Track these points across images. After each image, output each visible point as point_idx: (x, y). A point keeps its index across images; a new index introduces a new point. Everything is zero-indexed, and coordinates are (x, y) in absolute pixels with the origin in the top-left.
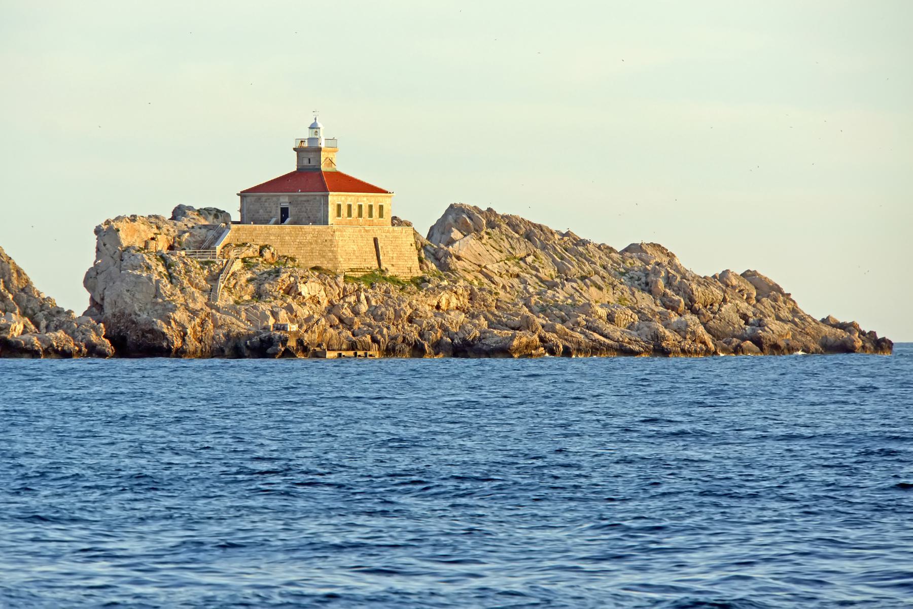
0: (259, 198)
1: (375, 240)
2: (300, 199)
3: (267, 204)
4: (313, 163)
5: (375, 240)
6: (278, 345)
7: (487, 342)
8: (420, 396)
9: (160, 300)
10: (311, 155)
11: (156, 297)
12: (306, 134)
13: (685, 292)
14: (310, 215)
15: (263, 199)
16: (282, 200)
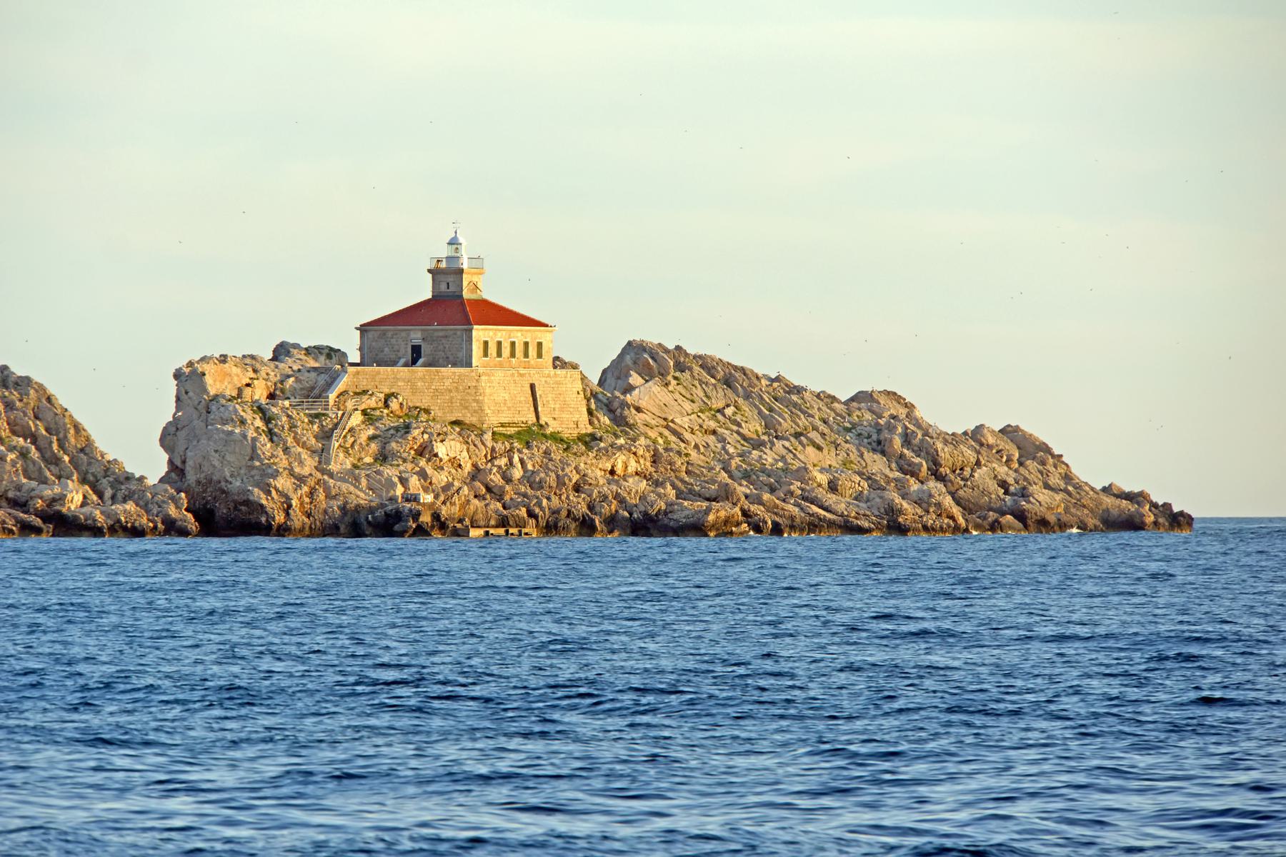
0: (384, 333)
1: (532, 387)
2: (436, 334)
3: (393, 341)
4: (452, 289)
5: (532, 387)
6: (407, 521)
9: (257, 464)
10: (451, 279)
12: (444, 252)
13: (927, 453)
14: (449, 354)
15: (389, 334)
16: (413, 335)
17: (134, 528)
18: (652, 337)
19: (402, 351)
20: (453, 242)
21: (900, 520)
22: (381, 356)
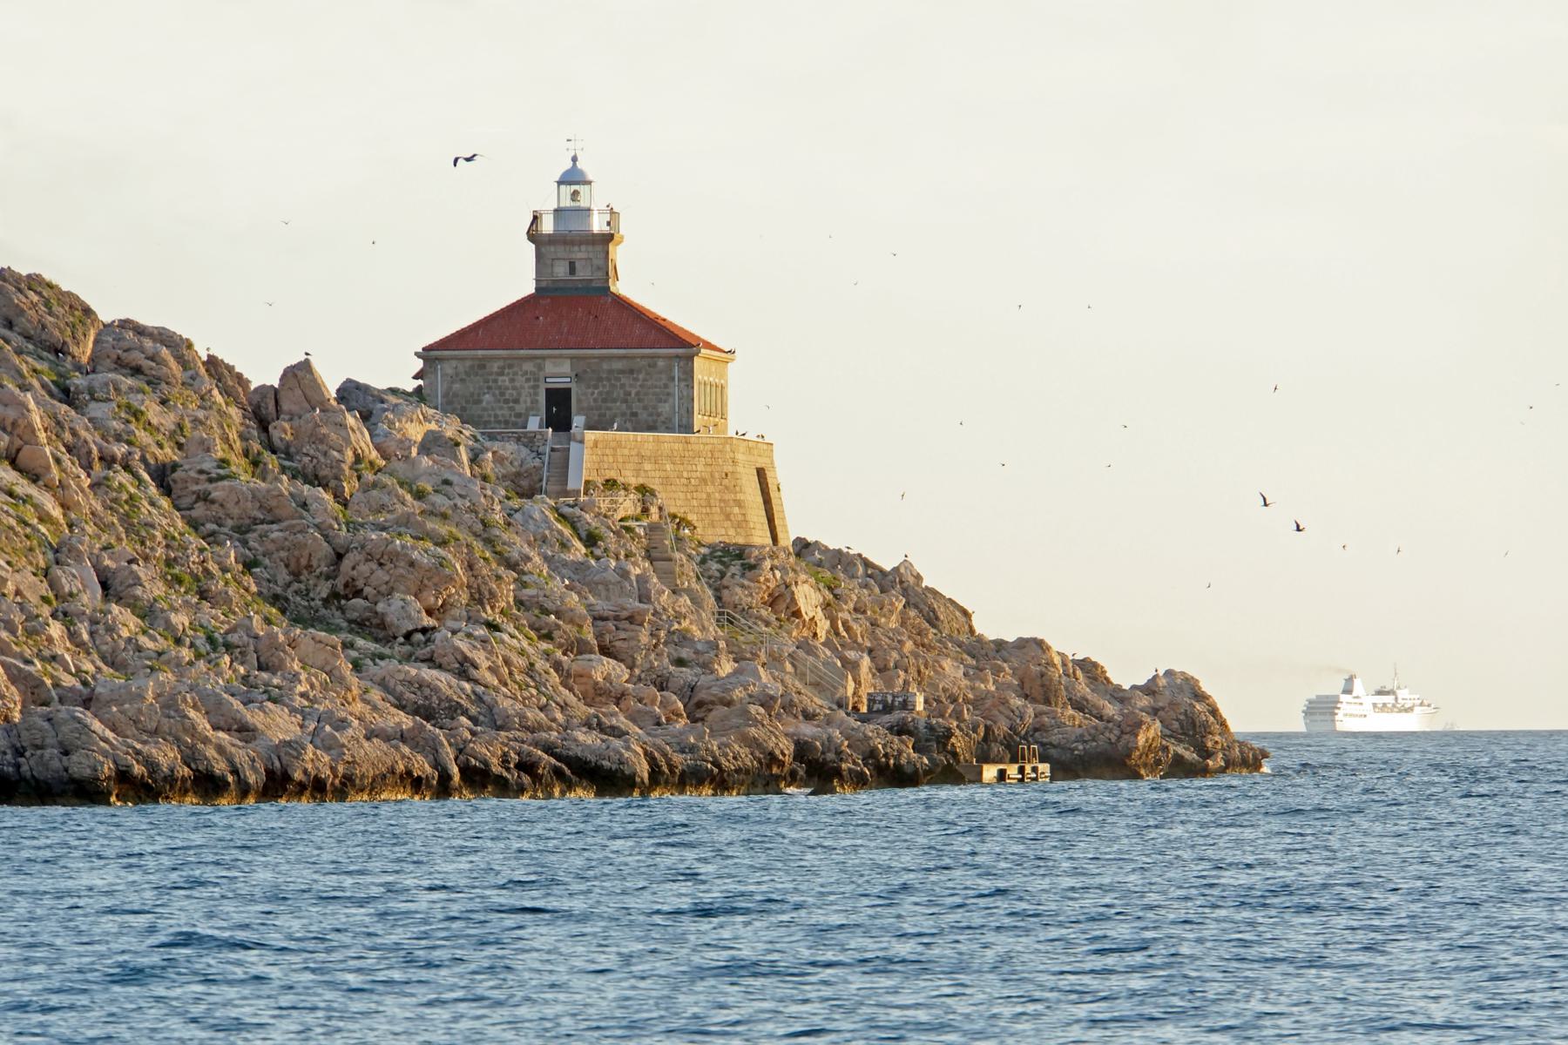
0: (482, 364)
2: (605, 366)
3: (504, 380)
4: (583, 273)
7: (1055, 739)
8: (896, 1013)
10: (580, 254)
12: (548, 199)
14: (637, 407)
16: (549, 367)
17: (898, 767)
18: (361, 379)
20: (573, 178)
21: (1210, 744)
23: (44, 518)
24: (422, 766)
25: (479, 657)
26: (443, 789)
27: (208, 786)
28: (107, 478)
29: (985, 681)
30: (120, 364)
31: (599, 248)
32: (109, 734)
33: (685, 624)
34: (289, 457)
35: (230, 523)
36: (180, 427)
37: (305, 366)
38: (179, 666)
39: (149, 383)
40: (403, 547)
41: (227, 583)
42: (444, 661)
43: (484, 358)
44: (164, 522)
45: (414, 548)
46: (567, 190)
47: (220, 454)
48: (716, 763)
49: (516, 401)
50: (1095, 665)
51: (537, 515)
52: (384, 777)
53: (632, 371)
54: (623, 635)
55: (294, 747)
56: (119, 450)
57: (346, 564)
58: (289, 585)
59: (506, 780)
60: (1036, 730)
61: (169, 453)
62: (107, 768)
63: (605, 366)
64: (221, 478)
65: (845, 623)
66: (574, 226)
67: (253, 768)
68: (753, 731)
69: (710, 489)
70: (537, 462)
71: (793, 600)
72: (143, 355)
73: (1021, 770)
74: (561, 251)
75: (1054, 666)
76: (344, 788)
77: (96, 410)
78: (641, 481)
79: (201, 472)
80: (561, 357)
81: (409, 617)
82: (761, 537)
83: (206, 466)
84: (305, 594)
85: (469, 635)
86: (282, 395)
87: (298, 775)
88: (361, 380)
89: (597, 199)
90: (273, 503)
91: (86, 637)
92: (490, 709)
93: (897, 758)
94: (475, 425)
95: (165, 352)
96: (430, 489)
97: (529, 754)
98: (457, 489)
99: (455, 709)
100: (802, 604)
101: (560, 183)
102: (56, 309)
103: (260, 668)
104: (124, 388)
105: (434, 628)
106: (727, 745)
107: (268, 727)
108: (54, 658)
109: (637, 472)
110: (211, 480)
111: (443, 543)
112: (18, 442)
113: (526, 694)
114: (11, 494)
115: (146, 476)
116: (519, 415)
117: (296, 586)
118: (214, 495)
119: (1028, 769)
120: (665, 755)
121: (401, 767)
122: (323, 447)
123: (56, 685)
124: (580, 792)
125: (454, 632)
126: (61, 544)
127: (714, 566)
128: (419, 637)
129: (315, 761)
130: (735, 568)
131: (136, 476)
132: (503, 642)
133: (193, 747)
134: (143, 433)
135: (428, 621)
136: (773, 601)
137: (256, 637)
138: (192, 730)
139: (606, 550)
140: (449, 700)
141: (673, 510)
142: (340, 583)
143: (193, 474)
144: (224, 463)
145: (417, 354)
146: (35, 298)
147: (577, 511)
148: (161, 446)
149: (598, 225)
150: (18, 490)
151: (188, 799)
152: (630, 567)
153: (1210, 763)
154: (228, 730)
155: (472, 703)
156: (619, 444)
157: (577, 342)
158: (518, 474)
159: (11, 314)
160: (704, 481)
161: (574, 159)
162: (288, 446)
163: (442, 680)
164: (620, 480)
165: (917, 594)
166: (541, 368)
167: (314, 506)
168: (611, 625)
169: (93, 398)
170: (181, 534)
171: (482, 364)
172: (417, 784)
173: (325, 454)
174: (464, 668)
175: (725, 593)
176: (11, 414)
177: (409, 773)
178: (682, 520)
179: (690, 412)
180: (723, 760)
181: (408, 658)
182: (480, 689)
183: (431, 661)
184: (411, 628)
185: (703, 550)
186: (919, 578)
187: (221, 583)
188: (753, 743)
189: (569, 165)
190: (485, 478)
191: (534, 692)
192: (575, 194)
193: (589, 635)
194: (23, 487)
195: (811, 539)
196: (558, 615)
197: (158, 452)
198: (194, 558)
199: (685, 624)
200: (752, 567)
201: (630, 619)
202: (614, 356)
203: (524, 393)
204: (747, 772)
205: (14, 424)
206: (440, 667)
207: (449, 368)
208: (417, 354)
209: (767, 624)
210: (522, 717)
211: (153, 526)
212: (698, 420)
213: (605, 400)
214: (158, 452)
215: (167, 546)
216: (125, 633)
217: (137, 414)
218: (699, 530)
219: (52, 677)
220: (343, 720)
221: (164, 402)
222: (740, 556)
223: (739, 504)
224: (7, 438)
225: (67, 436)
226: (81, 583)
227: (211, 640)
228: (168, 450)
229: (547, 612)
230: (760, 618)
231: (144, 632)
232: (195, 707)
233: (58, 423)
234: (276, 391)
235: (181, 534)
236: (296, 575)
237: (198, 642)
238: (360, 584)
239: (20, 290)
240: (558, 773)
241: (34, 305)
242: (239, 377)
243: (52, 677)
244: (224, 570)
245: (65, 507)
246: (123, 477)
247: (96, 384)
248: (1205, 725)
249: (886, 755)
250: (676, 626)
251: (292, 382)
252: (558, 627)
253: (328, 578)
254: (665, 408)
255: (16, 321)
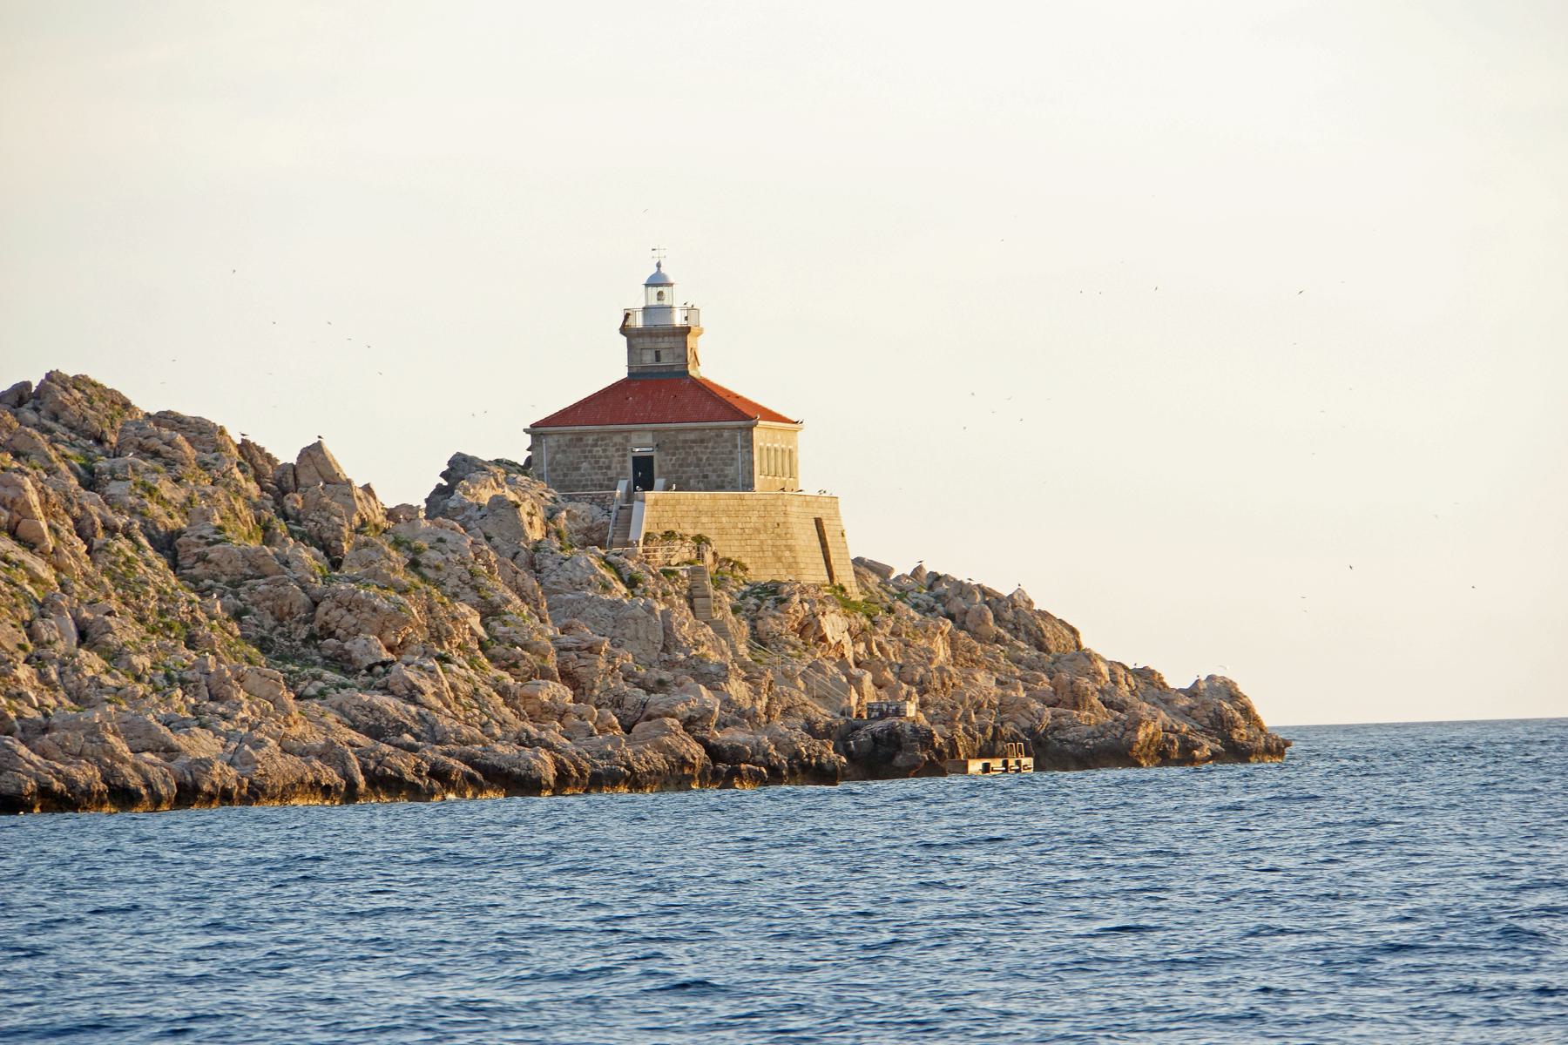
1: (818, 522)
2: (681, 437)
3: (598, 451)
4: (666, 361)
5: (818, 522)
6: (913, 749)
7: (1069, 736)
9: (682, 656)
10: (663, 344)
11: (665, 649)
12: (638, 299)
13: (1028, 633)
14: (708, 470)
15: (590, 440)
16: (634, 438)
17: (820, 765)
18: (469, 452)
19: (616, 467)
20: (657, 281)
21: (1235, 736)
22: (575, 476)
23: (35, 579)
24: (330, 776)
25: (426, 685)
26: (351, 795)
27: (123, 797)
28: (106, 545)
29: (1015, 689)
30: (142, 450)
31: (679, 339)
32: (35, 758)
33: (703, 650)
34: (299, 522)
35: (224, 578)
36: (190, 500)
37: (318, 447)
38: (134, 699)
39: (166, 464)
40: (367, 595)
41: (212, 629)
42: (396, 688)
43: (581, 433)
44: (158, 579)
45: (376, 596)
46: (655, 290)
47: (219, 522)
48: (629, 767)
49: (609, 468)
50: (1153, 672)
51: (583, 563)
52: (293, 786)
53: (702, 441)
54: (583, 662)
55: (206, 764)
56: (121, 521)
57: (321, 610)
58: (274, 629)
59: (418, 786)
60: (1056, 729)
61: (178, 522)
62: (30, 785)
63: (681, 437)
64: (217, 542)
65: (879, 645)
66: (660, 321)
67: (165, 782)
68: (667, 740)
69: (763, 537)
70: (605, 519)
71: (820, 628)
72: (184, 441)
73: (1005, 764)
74: (647, 342)
75: (1101, 674)
76: (255, 793)
77: (114, 488)
78: (698, 532)
79: (201, 537)
80: (643, 430)
81: (370, 653)
82: (814, 574)
83: (204, 533)
84: (288, 636)
85: (420, 667)
86: (299, 471)
87: (206, 787)
88: (469, 453)
89: (677, 298)
90: (261, 562)
91: (54, 676)
92: (432, 727)
93: (818, 758)
94: (559, 488)
95: (179, 438)
96: (426, 546)
97: (443, 764)
98: (450, 546)
99: (401, 728)
100: (828, 630)
101: (647, 285)
102: (99, 404)
103: (212, 699)
104: (141, 469)
105: (392, 662)
106: (641, 752)
107: (192, 748)
108: (20, 695)
109: (695, 525)
110: (209, 544)
111: (404, 591)
112: (17, 517)
113: (469, 714)
114: (5, 560)
115: (144, 541)
116: (611, 479)
117: (280, 629)
118: (211, 556)
119: (1012, 762)
120: (575, 762)
121: (310, 777)
122: (326, 514)
123: (19, 718)
124: (491, 794)
125: (407, 665)
126: (46, 600)
127: (752, 601)
128: (380, 669)
129: (224, 774)
130: (769, 602)
131: (135, 541)
132: (451, 671)
133: (111, 767)
134: (155, 506)
135: (386, 656)
136: (802, 630)
137: (208, 674)
138: (112, 752)
139: (645, 590)
140: (396, 721)
141: (728, 555)
142: (316, 626)
143: (194, 539)
144: (220, 529)
145: (526, 431)
146: (78, 395)
147: (622, 559)
148: (171, 516)
149: (678, 320)
150: (12, 556)
151: (106, 809)
152: (656, 605)
153: (1197, 753)
154: (154, 751)
155: (416, 722)
156: (678, 502)
157: (663, 413)
158: (590, 529)
159: (57, 408)
160: (757, 530)
161: (659, 265)
162: (299, 513)
163: (391, 704)
164: (678, 531)
165: (1026, 617)
166: (628, 440)
167: (295, 564)
168: (573, 655)
169: (114, 478)
170: (174, 589)
171: (579, 438)
172: (327, 791)
173: (328, 519)
174: (412, 694)
175: (760, 622)
176: (10, 494)
177: (318, 782)
178: (736, 563)
179: (751, 473)
180: (635, 765)
181: (368, 687)
182: (424, 711)
183: (386, 690)
184: (372, 662)
185: (745, 588)
186: (1030, 602)
187: (207, 629)
188: (661, 748)
189: (655, 270)
190: (559, 534)
191: (477, 712)
192: (660, 294)
193: (552, 663)
194: (18, 553)
195: (941, 573)
196: (524, 647)
197: (168, 521)
198: (184, 609)
199: (703, 650)
200: (783, 601)
201: (590, 649)
202: (689, 429)
203: (615, 460)
204: (659, 773)
205: (13, 502)
206: (392, 693)
207: (552, 441)
208: (526, 431)
209: (795, 647)
210: (458, 733)
211: (147, 583)
212: (758, 479)
213: (681, 466)
214: (168, 521)
215: (160, 599)
216: (89, 673)
217: (151, 491)
218: (752, 571)
219: (16, 711)
220: (261, 741)
221: (177, 480)
222: (774, 592)
223: (790, 548)
224: (7, 514)
225: (76, 511)
226: (59, 634)
227: (168, 677)
228: (178, 520)
229: (514, 645)
230: (788, 643)
231: (108, 672)
232: (115, 733)
233: (68, 500)
234: (294, 468)
235: (174, 589)
236: (280, 621)
237: (156, 679)
238: (333, 626)
239: (66, 389)
240: (471, 779)
241: (77, 401)
242: (269, 456)
243: (16, 711)
244: (211, 618)
245: (59, 569)
246: (123, 544)
247: (117, 466)
248: (1232, 721)
249: (809, 756)
250: (694, 652)
251: (307, 461)
252: (523, 657)
253: (306, 622)
254: (730, 471)
255: (61, 414)
